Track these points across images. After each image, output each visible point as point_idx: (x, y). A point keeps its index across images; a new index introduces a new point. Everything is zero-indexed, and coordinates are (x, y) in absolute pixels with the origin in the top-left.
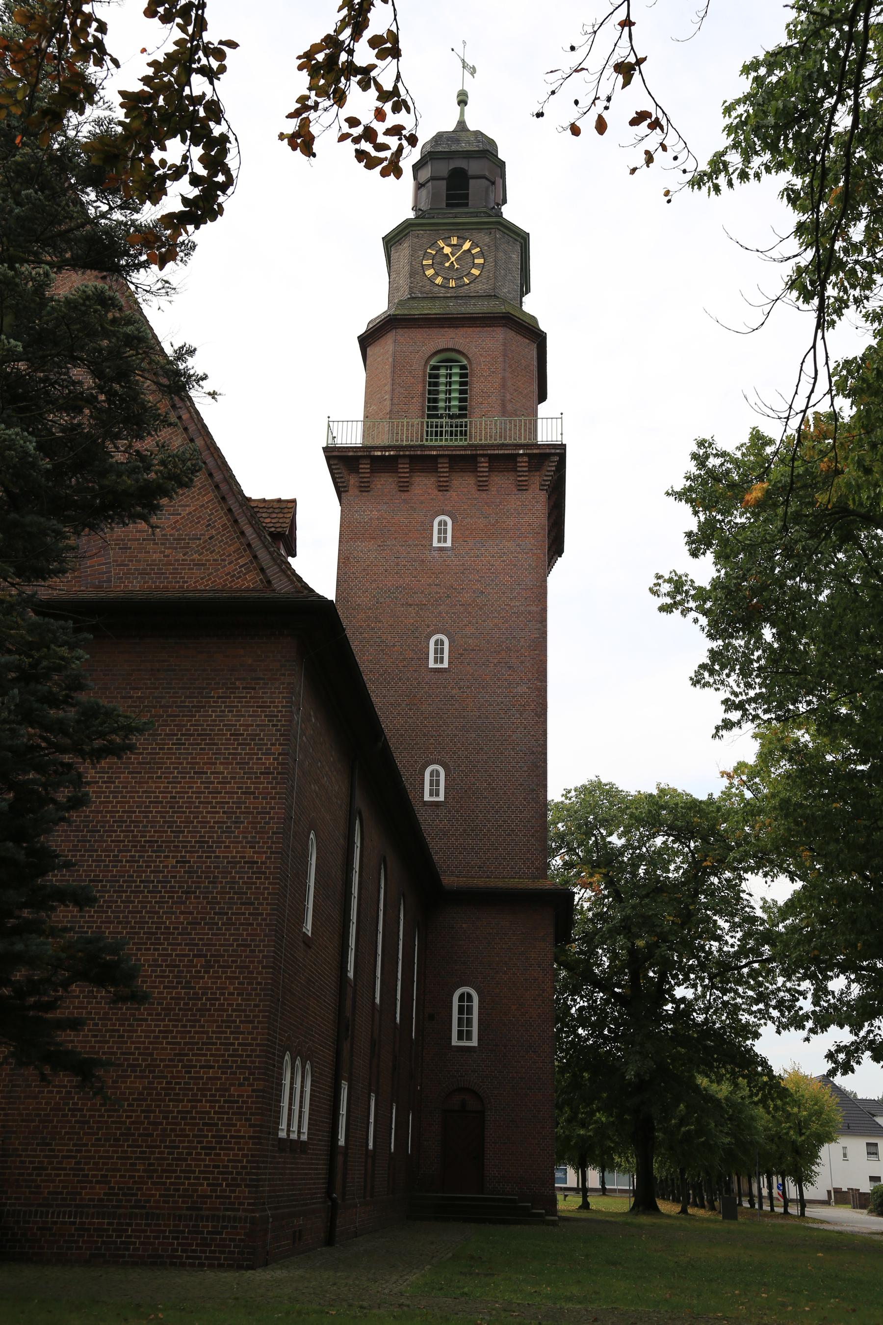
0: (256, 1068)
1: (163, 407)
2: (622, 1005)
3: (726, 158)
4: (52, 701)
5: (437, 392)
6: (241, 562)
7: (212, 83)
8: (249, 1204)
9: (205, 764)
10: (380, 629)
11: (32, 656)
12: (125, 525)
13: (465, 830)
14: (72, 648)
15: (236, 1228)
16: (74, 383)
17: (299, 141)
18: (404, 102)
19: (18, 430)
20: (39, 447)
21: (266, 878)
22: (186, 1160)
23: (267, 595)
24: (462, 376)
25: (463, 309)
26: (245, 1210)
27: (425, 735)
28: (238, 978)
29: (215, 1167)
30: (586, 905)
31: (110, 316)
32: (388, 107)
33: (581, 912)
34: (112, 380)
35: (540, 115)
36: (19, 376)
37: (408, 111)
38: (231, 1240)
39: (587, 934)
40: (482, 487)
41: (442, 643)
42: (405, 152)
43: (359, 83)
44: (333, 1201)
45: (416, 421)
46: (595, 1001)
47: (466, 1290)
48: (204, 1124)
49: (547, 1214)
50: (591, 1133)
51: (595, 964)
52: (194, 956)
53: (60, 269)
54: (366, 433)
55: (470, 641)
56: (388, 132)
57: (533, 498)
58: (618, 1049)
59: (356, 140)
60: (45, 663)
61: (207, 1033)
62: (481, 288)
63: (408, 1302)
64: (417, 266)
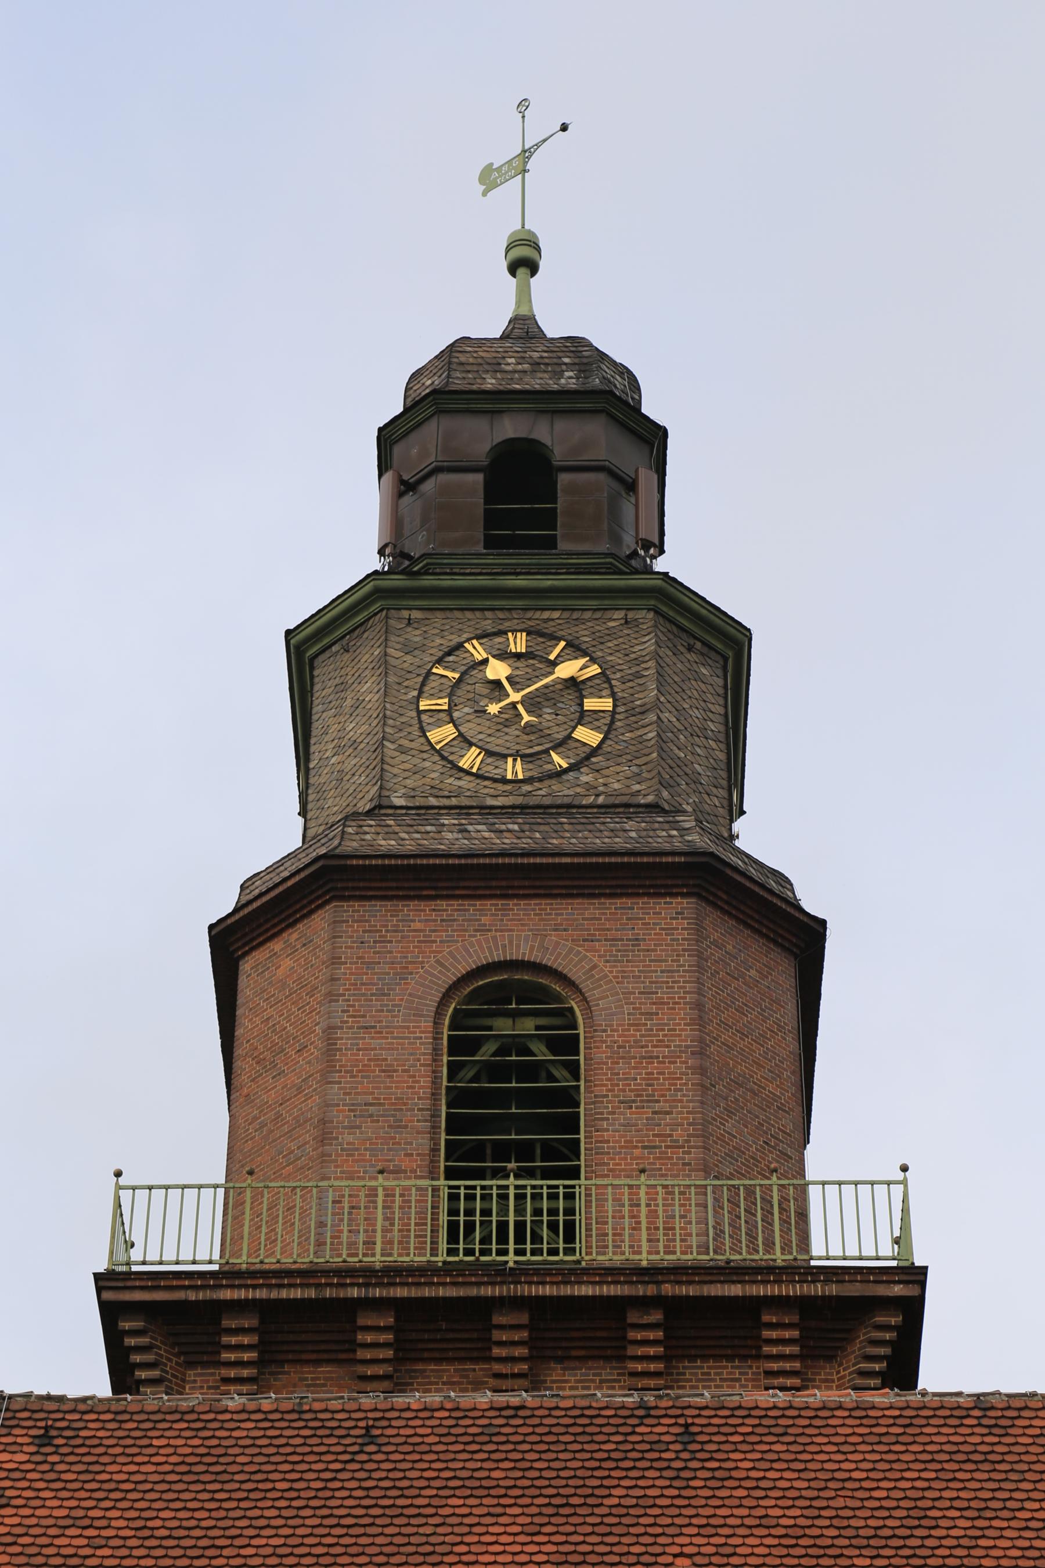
54: (230, 1239)
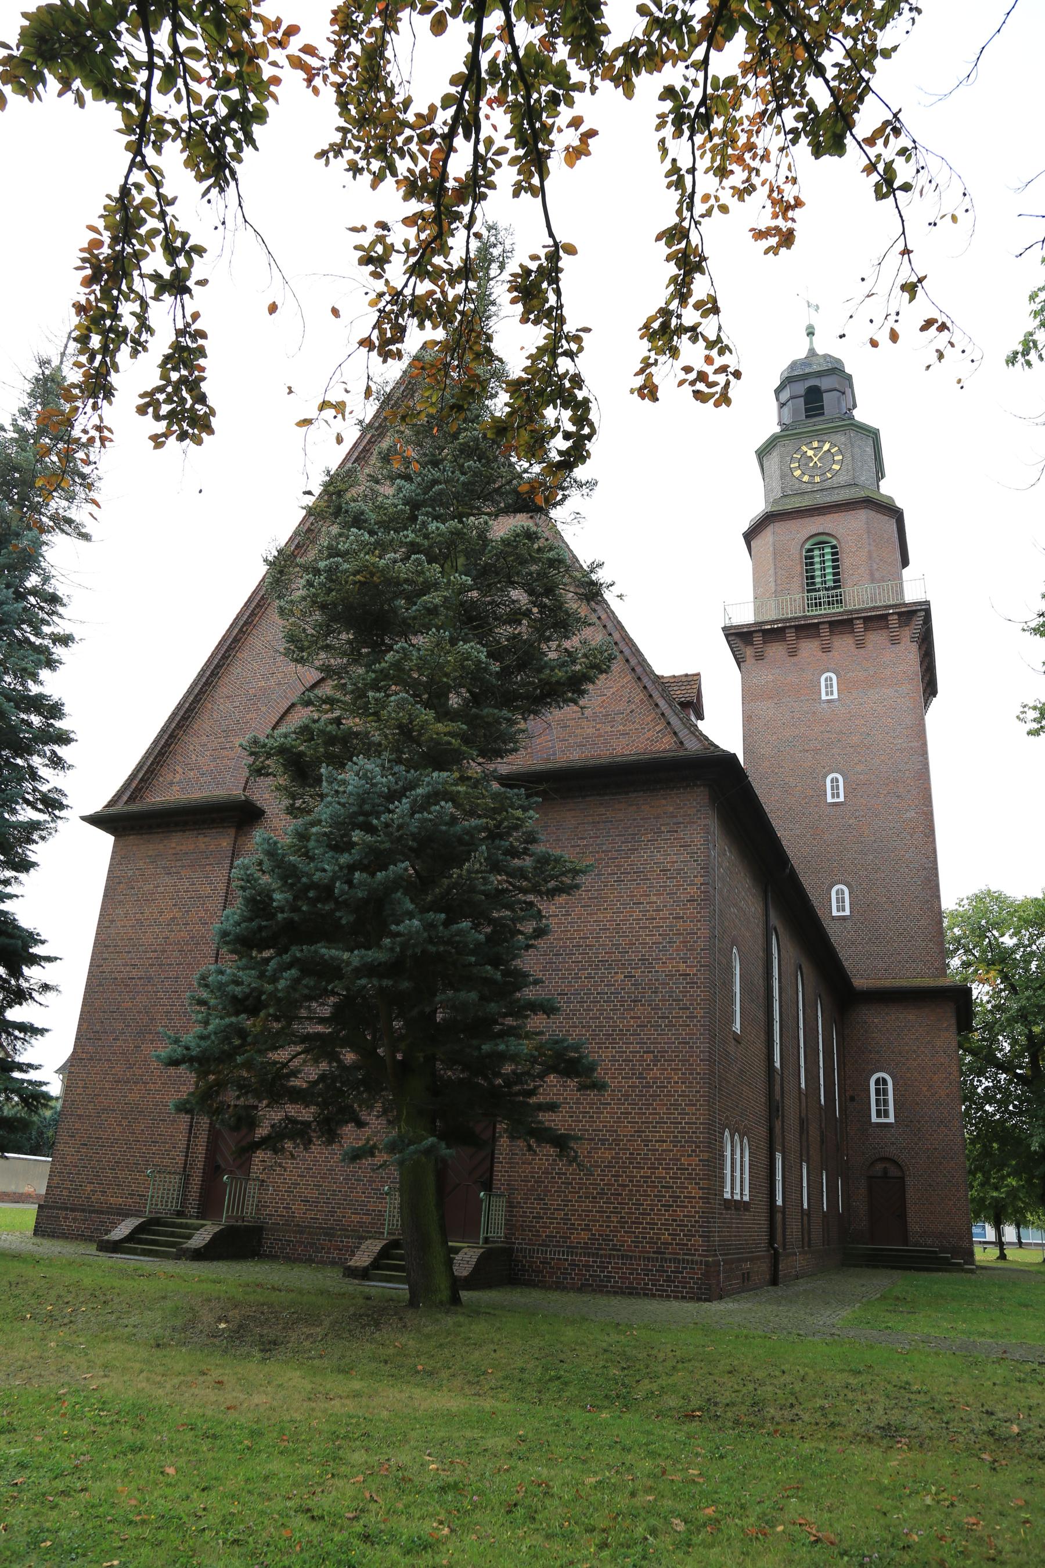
0: (700, 1142)
1: (583, 610)
2: (1024, 1084)
3: (1035, 337)
4: (513, 853)
5: (814, 570)
6: (658, 728)
7: (573, 361)
8: (703, 1251)
9: (641, 896)
10: (782, 773)
11: (495, 819)
12: (561, 708)
13: (870, 939)
14: (525, 809)
15: (693, 1269)
16: (514, 602)
17: (646, 391)
18: (727, 347)
19: (472, 644)
20: (490, 655)
21: (698, 987)
22: (649, 1214)
23: (680, 754)
24: (833, 554)
25: (828, 499)
26: (699, 1255)
27: (828, 860)
28: (681, 1069)
29: (673, 1220)
30: (985, 999)
31: (536, 546)
32: (714, 353)
33: (981, 1005)
34: (542, 595)
35: (842, 336)
36: (473, 602)
37: (731, 352)
38: (691, 1278)
39: (987, 1024)
40: (860, 645)
41: (837, 781)
42: (731, 385)
43: (689, 339)
44: (775, 1249)
45: (798, 596)
46: (999, 1081)
47: (889, 1325)
48: (662, 1187)
49: (966, 1263)
50: (1003, 1196)
51: (997, 1049)
52: (644, 1052)
53: (497, 516)
54: (757, 610)
55: (862, 777)
56: (716, 372)
57: (906, 649)
58: (1024, 1123)
59: (692, 383)
60: (506, 824)
61: (659, 1114)
62: (842, 479)
63: (838, 1333)
64: (787, 470)
